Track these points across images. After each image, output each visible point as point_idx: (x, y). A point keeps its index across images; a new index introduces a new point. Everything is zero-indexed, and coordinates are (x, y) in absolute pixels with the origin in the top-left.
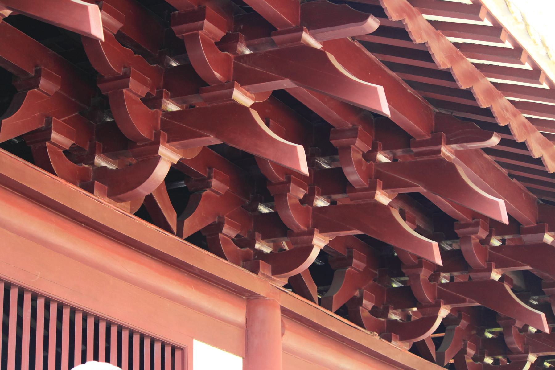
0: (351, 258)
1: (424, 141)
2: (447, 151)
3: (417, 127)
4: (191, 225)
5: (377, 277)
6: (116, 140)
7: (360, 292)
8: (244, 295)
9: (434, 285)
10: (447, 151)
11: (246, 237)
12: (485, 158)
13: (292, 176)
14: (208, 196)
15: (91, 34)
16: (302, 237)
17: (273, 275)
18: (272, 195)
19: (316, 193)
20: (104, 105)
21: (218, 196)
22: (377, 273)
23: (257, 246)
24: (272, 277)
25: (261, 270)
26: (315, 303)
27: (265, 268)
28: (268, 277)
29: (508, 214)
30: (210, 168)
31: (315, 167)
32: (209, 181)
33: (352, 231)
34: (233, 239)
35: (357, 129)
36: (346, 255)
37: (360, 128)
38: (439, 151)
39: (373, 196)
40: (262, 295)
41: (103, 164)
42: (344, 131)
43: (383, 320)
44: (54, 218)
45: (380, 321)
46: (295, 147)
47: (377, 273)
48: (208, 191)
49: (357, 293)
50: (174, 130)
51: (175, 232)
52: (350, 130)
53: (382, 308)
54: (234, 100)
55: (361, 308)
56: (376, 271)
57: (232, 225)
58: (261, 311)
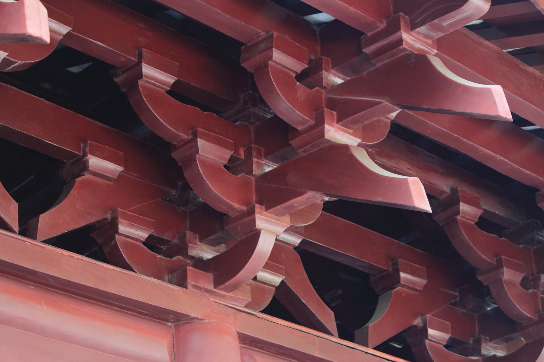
0: (396, 272)
1: (378, 32)
2: (413, 40)
3: (352, 9)
4: (50, 222)
5: (458, 299)
6: (209, 220)
7: (422, 319)
8: (168, 321)
9: (535, 295)
10: (413, 40)
11: (176, 241)
12: (526, 71)
13: (503, 257)
14: (87, 183)
15: (415, 207)
16: (241, 221)
17: (215, 287)
18: (180, 164)
19: (254, 153)
20: (482, 292)
21: (111, 183)
22: (457, 294)
23: (484, 352)
24: (215, 290)
25: (190, 281)
26: (332, 335)
27: (206, 281)
28: (207, 291)
29: (512, 113)
30: (85, 141)
31: (251, 120)
32: (84, 159)
33: (306, 195)
34: (144, 243)
35: (272, 35)
36: (391, 270)
37: (275, 34)
38: (400, 41)
39: (322, 134)
40: (193, 315)
41: (492, 353)
42: (257, 44)
43: (477, 358)
44: (105, 313)
45: (471, 360)
46: (407, 179)
47: (457, 294)
48: (87, 176)
49: (418, 322)
50: (273, 194)
51: (17, 229)
52: (263, 40)
53: (471, 342)
54: (329, 141)
55: (427, 342)
56: (456, 291)
57: (133, 221)
58: (197, 341)
